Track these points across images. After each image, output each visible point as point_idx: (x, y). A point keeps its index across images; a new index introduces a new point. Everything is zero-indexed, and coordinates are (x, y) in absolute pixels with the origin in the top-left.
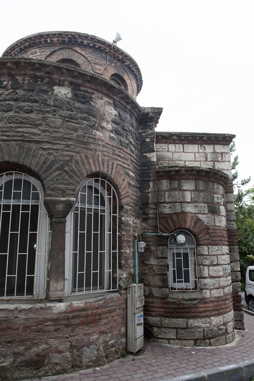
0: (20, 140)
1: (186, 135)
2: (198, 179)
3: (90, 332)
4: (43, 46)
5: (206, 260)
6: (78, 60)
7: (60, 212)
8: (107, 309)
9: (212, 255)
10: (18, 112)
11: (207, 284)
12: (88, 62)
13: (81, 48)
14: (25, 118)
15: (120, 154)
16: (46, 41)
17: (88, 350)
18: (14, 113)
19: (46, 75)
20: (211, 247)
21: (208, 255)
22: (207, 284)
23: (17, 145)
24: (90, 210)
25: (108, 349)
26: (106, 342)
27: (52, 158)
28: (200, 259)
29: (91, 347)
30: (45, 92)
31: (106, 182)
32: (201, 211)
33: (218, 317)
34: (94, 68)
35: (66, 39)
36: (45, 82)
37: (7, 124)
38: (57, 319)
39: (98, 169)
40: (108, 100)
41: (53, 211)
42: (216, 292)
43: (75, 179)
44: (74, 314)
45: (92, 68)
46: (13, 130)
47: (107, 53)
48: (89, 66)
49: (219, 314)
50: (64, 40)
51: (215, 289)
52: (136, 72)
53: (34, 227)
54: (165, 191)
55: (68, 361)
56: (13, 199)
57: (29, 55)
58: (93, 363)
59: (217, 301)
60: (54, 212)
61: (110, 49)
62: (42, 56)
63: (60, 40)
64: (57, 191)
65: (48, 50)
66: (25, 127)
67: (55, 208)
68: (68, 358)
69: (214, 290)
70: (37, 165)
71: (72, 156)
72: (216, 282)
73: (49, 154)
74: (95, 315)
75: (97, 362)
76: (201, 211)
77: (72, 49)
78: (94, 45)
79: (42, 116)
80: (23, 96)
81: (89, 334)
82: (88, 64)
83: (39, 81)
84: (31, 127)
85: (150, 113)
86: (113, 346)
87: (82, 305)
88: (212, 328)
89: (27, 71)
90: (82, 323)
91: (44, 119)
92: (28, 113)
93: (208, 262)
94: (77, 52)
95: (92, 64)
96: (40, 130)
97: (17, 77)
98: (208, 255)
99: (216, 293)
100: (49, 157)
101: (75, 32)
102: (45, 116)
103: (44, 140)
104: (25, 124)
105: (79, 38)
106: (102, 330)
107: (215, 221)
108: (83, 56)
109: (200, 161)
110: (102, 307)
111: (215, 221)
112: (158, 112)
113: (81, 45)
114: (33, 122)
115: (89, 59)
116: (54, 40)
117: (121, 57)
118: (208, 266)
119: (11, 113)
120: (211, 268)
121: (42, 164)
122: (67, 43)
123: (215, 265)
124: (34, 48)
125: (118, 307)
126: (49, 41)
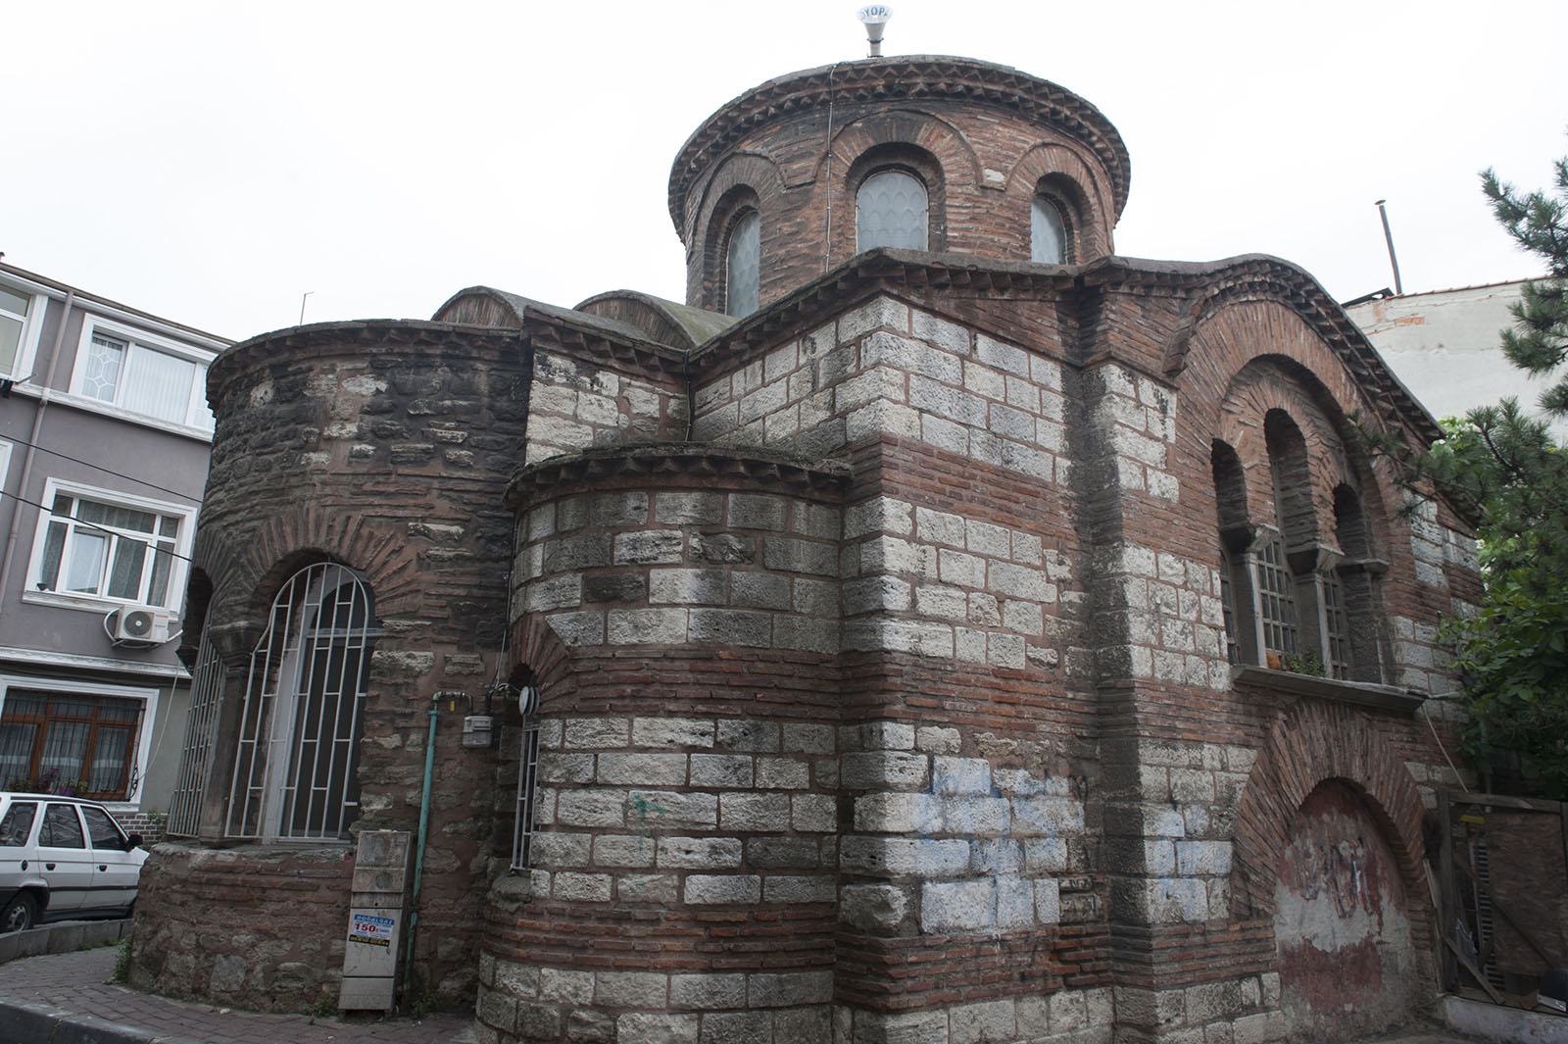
1: (754, 325)
2: (562, 497)
3: (233, 922)
5: (555, 767)
8: (285, 880)
9: (574, 751)
11: (543, 851)
15: (381, 488)
16: (690, 171)
17: (225, 963)
20: (573, 721)
21: (561, 750)
22: (543, 851)
25: (276, 979)
26: (276, 961)
28: (751, 771)
29: (232, 957)
32: (561, 601)
33: (572, 973)
38: (186, 880)
40: (350, 367)
42: (570, 882)
44: (211, 876)
47: (825, 103)
49: (577, 965)
51: (570, 869)
52: (980, 87)
55: (189, 976)
56: (320, 627)
58: (234, 998)
59: (572, 917)
68: (188, 968)
69: (567, 874)
71: (254, 529)
72: (578, 848)
74: (253, 888)
75: (241, 999)
76: (561, 601)
78: (780, 107)
81: (231, 927)
86: (292, 975)
87: (231, 859)
88: (540, 1005)
90: (222, 900)
93: (557, 773)
94: (746, 154)
98: (561, 750)
99: (570, 886)
106: (262, 926)
107: (606, 629)
110: (270, 871)
111: (606, 629)
117: (880, 85)
118: (559, 788)
120: (566, 795)
123: (586, 786)
125: (328, 883)
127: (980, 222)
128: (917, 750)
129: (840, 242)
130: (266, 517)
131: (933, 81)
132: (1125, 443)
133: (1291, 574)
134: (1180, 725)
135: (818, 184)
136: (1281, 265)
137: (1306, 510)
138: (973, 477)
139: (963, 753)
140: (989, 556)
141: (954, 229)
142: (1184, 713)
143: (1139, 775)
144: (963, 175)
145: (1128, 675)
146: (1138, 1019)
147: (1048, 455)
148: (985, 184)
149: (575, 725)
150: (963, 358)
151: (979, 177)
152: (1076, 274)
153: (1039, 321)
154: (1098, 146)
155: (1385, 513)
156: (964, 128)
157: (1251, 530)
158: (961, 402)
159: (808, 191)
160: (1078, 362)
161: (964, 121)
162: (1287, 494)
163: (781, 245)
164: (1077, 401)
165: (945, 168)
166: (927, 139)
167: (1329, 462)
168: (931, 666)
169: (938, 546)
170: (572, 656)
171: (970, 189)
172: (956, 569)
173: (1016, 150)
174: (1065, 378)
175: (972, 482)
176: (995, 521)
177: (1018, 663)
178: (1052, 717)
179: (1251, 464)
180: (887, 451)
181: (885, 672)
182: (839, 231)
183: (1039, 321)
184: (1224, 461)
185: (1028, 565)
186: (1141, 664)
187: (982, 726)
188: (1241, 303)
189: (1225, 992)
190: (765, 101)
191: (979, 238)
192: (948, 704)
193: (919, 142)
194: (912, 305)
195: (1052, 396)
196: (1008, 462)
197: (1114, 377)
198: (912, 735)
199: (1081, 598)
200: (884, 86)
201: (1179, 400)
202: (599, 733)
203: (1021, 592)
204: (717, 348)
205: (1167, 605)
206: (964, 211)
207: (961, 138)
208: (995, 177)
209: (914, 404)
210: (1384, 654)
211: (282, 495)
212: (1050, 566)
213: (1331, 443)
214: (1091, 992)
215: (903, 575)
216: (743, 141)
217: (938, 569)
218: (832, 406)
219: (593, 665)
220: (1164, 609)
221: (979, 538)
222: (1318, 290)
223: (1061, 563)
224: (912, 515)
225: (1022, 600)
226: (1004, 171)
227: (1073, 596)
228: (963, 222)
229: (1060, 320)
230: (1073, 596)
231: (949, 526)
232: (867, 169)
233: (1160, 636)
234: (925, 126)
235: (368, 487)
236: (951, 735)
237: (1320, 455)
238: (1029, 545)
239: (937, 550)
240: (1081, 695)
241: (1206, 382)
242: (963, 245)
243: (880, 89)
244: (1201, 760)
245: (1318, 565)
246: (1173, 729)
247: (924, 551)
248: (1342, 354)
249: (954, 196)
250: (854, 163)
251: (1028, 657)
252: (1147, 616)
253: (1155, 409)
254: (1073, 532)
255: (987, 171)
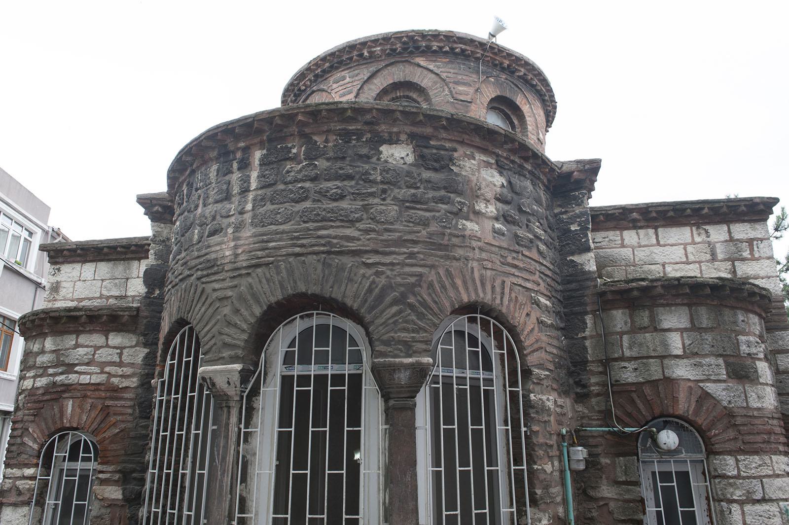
0: (323, 252)
4: (356, 65)
6: (422, 82)
7: (403, 387)
9: (748, 478)
10: (319, 201)
12: (442, 83)
13: (426, 58)
14: (332, 211)
15: (516, 262)
16: (361, 55)
18: (311, 203)
19: (366, 128)
21: (738, 477)
23: (319, 261)
24: (461, 380)
27: (382, 281)
30: (365, 159)
31: (492, 321)
32: (711, 375)
34: (454, 92)
35: (398, 46)
36: (364, 140)
37: (300, 225)
39: (473, 297)
40: (485, 159)
41: (390, 385)
43: (428, 319)
45: (451, 92)
46: (310, 234)
47: (478, 59)
48: (444, 90)
50: (394, 47)
52: (540, 87)
53: (355, 420)
54: (622, 334)
57: (331, 83)
60: (393, 388)
61: (484, 50)
62: (355, 84)
63: (387, 49)
64: (395, 345)
65: (365, 71)
66: (332, 227)
67: (394, 379)
70: (356, 297)
71: (420, 275)
73: (378, 274)
76: (711, 375)
77: (410, 62)
78: (452, 49)
79: (361, 203)
80: (325, 170)
82: (443, 86)
83: (354, 140)
84: (343, 227)
85: (574, 172)
89: (332, 124)
91: (366, 208)
92: (335, 200)
94: (419, 65)
95: (451, 85)
96: (360, 230)
97: (315, 138)
98: (738, 477)
100: (377, 280)
101: (413, 31)
102: (366, 202)
103: (368, 248)
104: (332, 221)
105: (421, 41)
108: (432, 71)
109: (700, 262)
111: (746, 396)
112: (591, 168)
113: (427, 52)
114: (346, 216)
115: (444, 75)
116: (375, 51)
117: (506, 63)
119: (308, 204)
120: (748, 508)
121: (365, 294)
122: (400, 53)
123: (758, 501)
124: (341, 70)
126: (366, 54)
130: (432, 267)
131: (527, 73)
149: (744, 460)
170: (730, 414)
190: (444, 41)
200: (508, 65)
202: (760, 466)
204: (619, 213)
211: (447, 251)
216: (418, 56)
219: (744, 420)
235: (509, 260)
243: (505, 65)
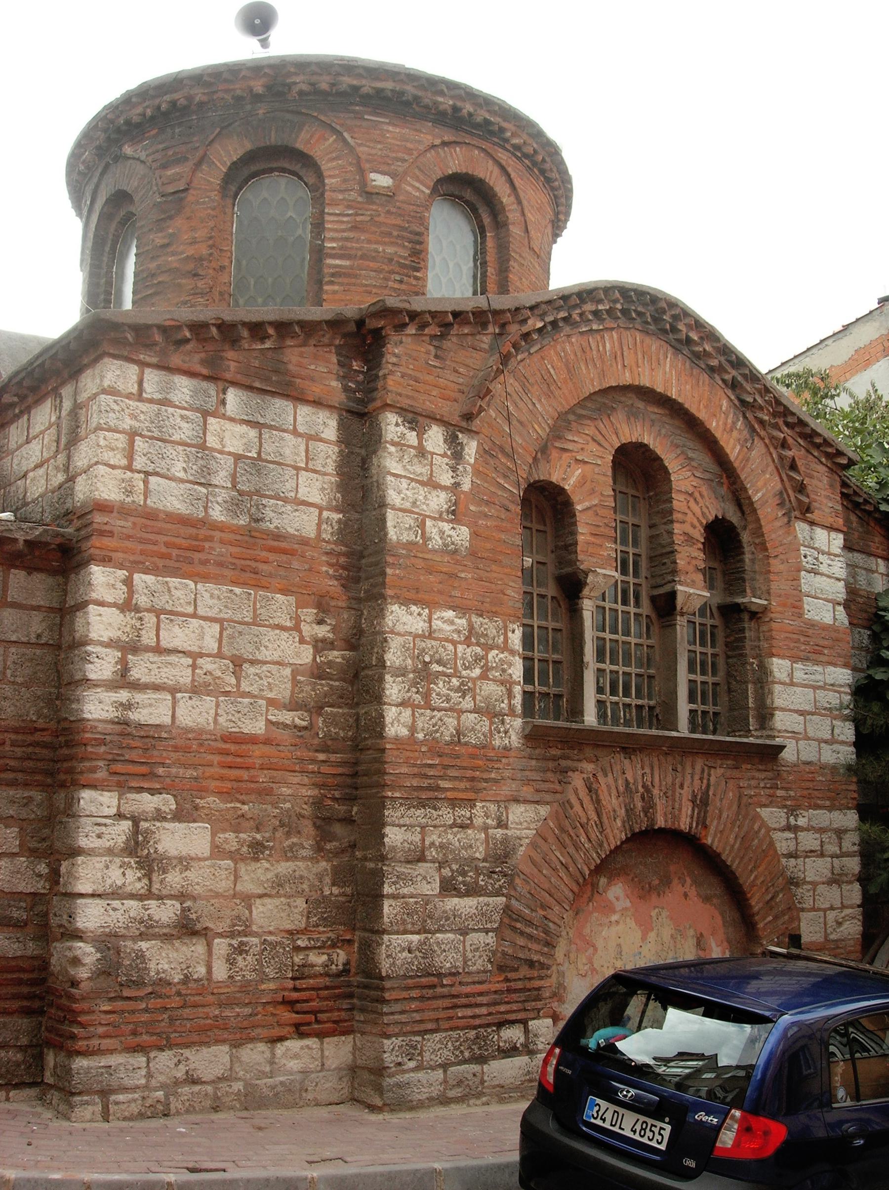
127: (363, 231)
128: (120, 816)
129: (211, 254)
132: (397, 493)
133: (654, 616)
134: (443, 784)
135: (191, 191)
136: (635, 290)
137: (668, 549)
138: (209, 539)
139: (179, 816)
140: (224, 620)
141: (333, 240)
142: (452, 773)
143: (383, 836)
144: (345, 181)
145: (381, 735)
146: (371, 1064)
147: (312, 509)
148: (368, 189)
150: (205, 414)
151: (363, 182)
152: (357, 317)
153: (313, 367)
154: (515, 141)
155: (766, 550)
156: (350, 130)
157: (581, 576)
158: (201, 462)
159: (181, 200)
160: (360, 408)
161: (349, 122)
162: (655, 532)
163: (152, 258)
164: (357, 450)
165: (325, 174)
166: (308, 142)
167: (702, 496)
168: (142, 733)
169: (158, 613)
171: (353, 195)
172: (176, 635)
173: (409, 151)
174: (342, 426)
175: (207, 545)
176: (235, 583)
177: (258, 727)
178: (296, 780)
179: (587, 504)
180: (99, 518)
181: (85, 741)
182: (211, 242)
183: (313, 367)
184: (547, 506)
185: (278, 627)
186: (396, 723)
187: (203, 791)
188: (582, 333)
189: (477, 1038)
191: (360, 249)
192: (161, 771)
193: (299, 145)
194: (143, 364)
195: (321, 446)
196: (257, 521)
197: (392, 426)
198: (115, 802)
199: (343, 658)
201: (480, 444)
203: (265, 654)
205: (439, 662)
206: (345, 219)
207: (344, 140)
208: (382, 181)
209: (139, 467)
210: (756, 700)
212: (305, 628)
213: (707, 476)
214: (327, 1040)
215: (111, 644)
217: (158, 636)
218: (67, 469)
220: (435, 667)
221: (211, 602)
222: (686, 313)
223: (320, 622)
224: (128, 582)
225: (266, 663)
226: (393, 175)
227: (335, 655)
228: (343, 231)
229: (340, 364)
230: (335, 655)
231: (173, 591)
232: (246, 172)
233: (427, 696)
234: (306, 127)
236: (167, 802)
237: (691, 490)
238: (281, 606)
239: (158, 617)
240: (333, 757)
241: (521, 423)
242: (341, 257)
244: (470, 818)
245: (678, 608)
246: (438, 788)
247: (141, 619)
248: (724, 381)
249: (335, 203)
250: (230, 169)
251: (267, 720)
252: (411, 676)
253: (444, 455)
254: (339, 589)
255: (373, 176)
